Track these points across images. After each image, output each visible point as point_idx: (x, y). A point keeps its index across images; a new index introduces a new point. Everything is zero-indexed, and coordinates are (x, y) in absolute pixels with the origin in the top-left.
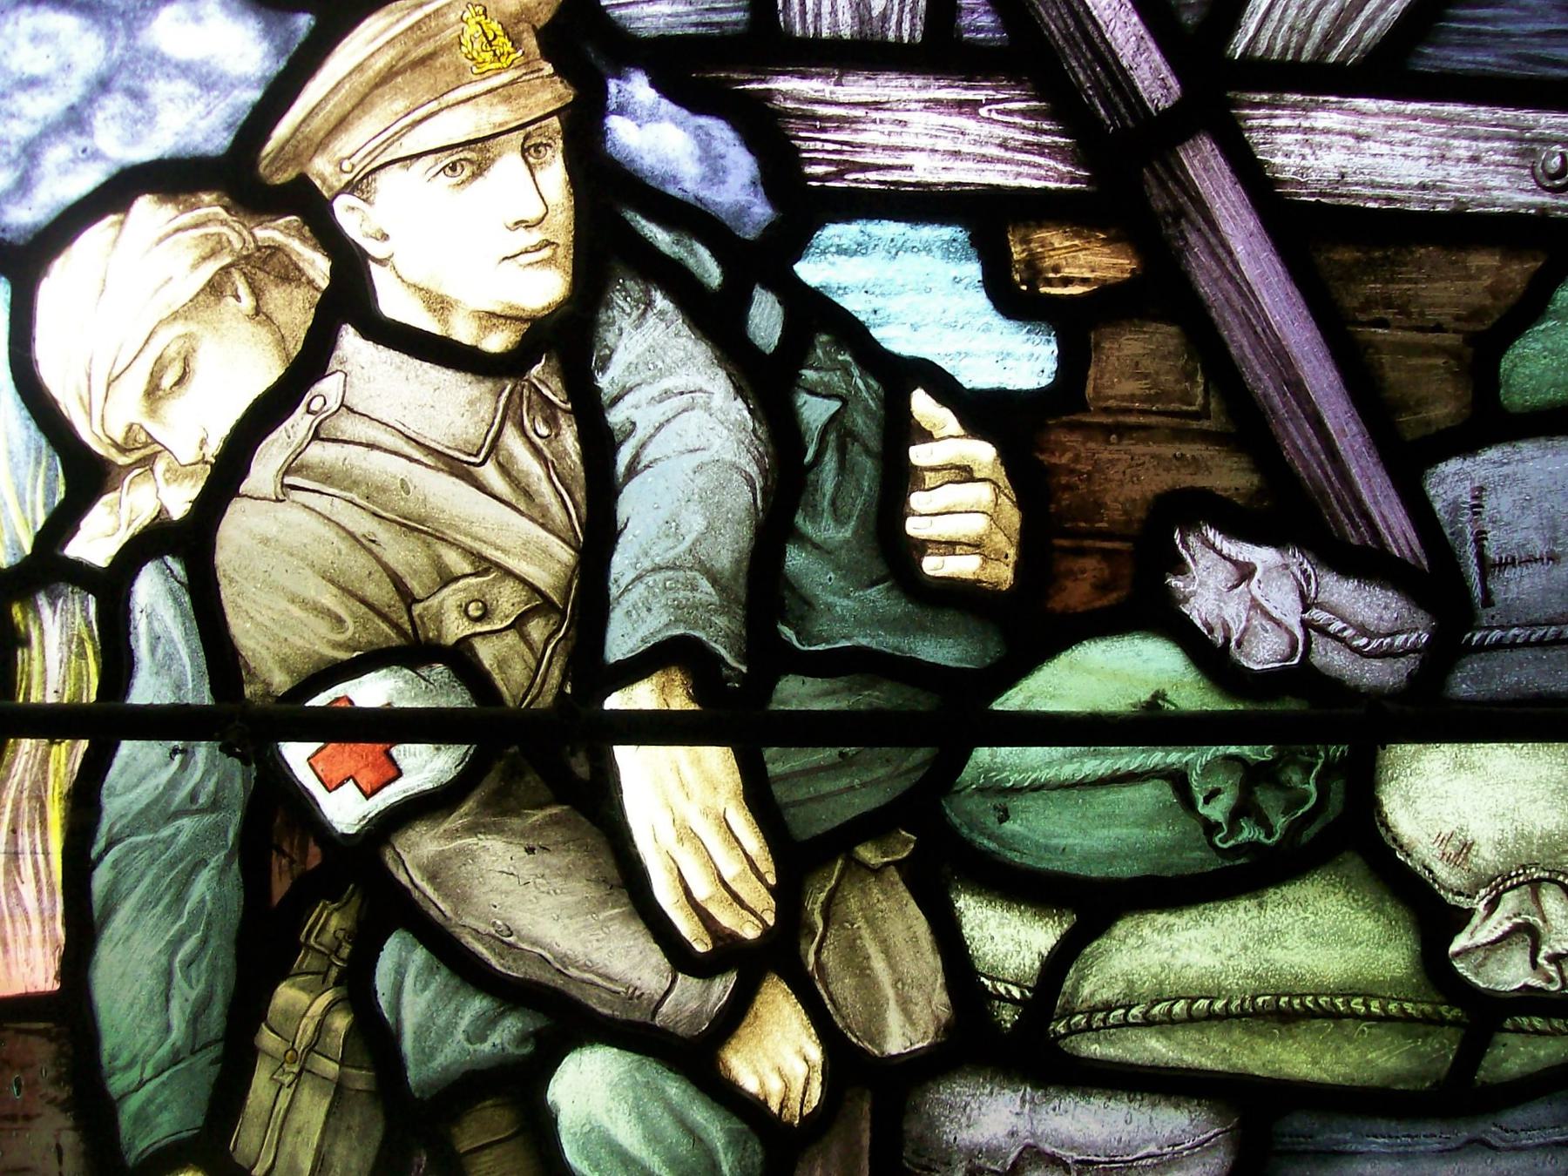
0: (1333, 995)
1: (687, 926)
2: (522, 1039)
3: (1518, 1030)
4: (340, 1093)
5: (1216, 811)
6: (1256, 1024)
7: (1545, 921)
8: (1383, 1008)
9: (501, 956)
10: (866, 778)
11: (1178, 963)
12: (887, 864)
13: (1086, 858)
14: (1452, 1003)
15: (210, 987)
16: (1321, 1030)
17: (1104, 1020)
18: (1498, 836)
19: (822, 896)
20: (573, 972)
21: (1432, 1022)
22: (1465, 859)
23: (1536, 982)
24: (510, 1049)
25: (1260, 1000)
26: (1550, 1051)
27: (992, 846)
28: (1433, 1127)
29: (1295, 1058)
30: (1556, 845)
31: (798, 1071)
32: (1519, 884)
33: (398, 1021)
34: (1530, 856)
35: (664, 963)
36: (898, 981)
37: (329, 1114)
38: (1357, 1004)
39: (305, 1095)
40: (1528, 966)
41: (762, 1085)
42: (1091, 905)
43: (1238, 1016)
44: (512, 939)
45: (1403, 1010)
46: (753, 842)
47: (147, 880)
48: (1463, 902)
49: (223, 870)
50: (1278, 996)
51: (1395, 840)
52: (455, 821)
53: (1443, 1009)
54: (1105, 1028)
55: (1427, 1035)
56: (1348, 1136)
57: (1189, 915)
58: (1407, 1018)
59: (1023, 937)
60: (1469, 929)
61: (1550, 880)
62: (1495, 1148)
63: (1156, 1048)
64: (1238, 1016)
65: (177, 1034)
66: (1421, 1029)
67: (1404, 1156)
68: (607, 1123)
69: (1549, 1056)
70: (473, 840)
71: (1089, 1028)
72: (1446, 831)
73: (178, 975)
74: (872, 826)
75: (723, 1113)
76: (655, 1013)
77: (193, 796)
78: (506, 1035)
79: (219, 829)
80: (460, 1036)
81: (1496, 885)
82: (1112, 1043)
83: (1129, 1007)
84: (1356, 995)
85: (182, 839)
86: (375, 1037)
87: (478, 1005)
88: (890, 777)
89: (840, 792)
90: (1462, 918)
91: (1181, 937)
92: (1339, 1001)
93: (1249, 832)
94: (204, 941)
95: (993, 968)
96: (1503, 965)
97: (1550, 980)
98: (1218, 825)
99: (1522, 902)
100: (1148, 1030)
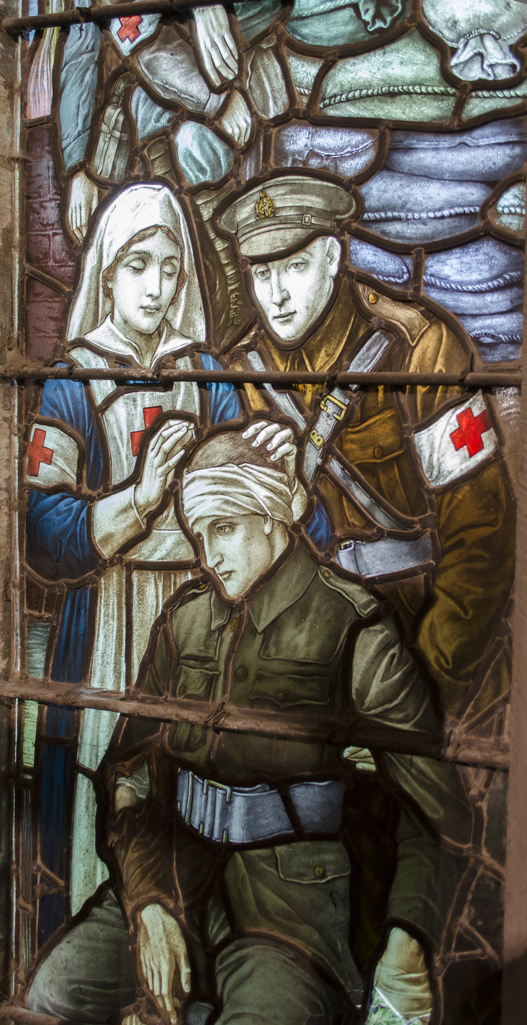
0: (408, 85)
1: (213, 76)
2: (169, 121)
3: (477, 97)
4: (120, 142)
5: (367, 17)
6: (382, 98)
7: (486, 50)
8: (427, 90)
9: (164, 92)
10: (264, 18)
11: (357, 77)
12: (268, 48)
13: (330, 39)
14: (453, 86)
15: (89, 112)
16: (405, 99)
17: (334, 101)
18: (466, 18)
19: (250, 62)
20: (183, 96)
21: (445, 94)
22: (455, 27)
23: (484, 76)
24: (166, 125)
25: (384, 89)
26: (490, 105)
27: (299, 38)
28: (448, 138)
29: (397, 111)
30: (489, 19)
31: (244, 125)
32: (476, 36)
33: (137, 117)
34: (479, 25)
35: (208, 91)
36: (273, 90)
37: (117, 150)
38: (417, 89)
39: (112, 143)
40: (480, 70)
41: (233, 131)
42: (330, 58)
43: (376, 96)
44: (167, 86)
45: (433, 90)
46: (231, 45)
47: (74, 76)
48: (454, 45)
49: (94, 71)
50: (389, 87)
51: (429, 22)
52: (154, 48)
53: (449, 89)
54: (335, 104)
55: (443, 100)
56: (415, 142)
57: (361, 58)
58: (435, 93)
59: (308, 71)
60: (457, 55)
61: (489, 34)
62: (470, 146)
63: (351, 111)
64: (376, 96)
65: (80, 127)
66: (440, 98)
67: (436, 149)
68: (190, 149)
69: (490, 107)
70: (158, 54)
71: (330, 105)
72: (448, 17)
73: (81, 107)
74: (264, 35)
75: (223, 143)
76: (204, 108)
77: (87, 48)
78: (165, 120)
79: (93, 57)
80: (153, 121)
81: (466, 36)
82: (337, 109)
83: (341, 95)
84: (416, 85)
85: (84, 61)
86: (129, 124)
87: (159, 109)
88: (270, 17)
89: (256, 25)
90: (454, 51)
91: (358, 67)
92: (411, 88)
93: (379, 24)
94: (88, 95)
95: (300, 83)
96: (470, 70)
97: (489, 75)
98: (368, 22)
99: (477, 43)
100: (347, 103)
